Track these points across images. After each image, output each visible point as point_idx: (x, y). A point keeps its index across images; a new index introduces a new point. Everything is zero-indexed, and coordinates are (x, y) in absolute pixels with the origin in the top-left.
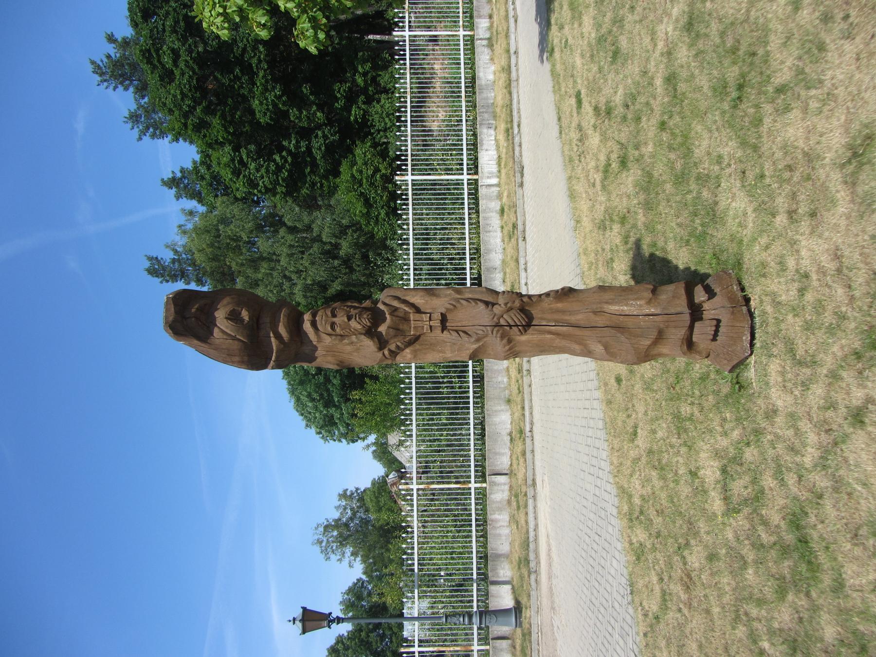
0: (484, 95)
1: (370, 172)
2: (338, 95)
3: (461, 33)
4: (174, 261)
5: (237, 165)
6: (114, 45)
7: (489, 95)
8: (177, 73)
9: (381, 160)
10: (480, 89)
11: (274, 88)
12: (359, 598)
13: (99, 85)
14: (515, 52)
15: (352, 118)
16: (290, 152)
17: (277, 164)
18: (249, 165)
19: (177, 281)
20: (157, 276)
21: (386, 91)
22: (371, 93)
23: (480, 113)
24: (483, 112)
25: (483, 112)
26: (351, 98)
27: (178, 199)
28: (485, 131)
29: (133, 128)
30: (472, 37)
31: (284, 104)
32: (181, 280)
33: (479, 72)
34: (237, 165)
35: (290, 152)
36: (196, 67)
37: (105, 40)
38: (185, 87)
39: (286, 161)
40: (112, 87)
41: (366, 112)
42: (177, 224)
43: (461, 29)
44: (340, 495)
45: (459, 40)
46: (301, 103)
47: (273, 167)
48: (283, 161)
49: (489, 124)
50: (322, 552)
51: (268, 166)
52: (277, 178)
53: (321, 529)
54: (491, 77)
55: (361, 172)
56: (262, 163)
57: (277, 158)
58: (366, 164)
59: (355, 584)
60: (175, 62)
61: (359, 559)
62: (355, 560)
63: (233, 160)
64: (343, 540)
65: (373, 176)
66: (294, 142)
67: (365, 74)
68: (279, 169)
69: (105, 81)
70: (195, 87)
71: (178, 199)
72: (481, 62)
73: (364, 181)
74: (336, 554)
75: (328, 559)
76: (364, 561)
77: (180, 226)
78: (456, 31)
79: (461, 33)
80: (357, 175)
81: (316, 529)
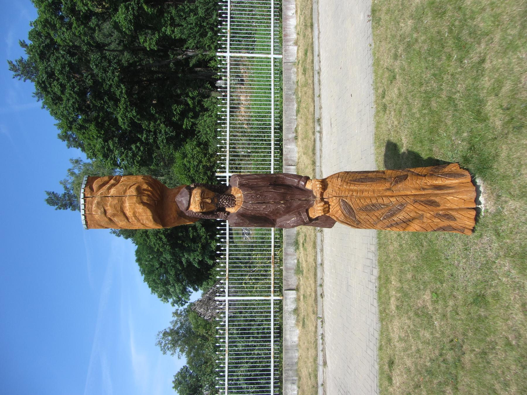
0: (290, 355)
1: (196, 163)
2: (175, 113)
3: (272, 298)
4: (65, 195)
5: (106, 151)
6: (25, 49)
7: (294, 355)
8: (65, 99)
9: (203, 156)
10: (286, 350)
11: (132, 110)
12: (184, 377)
13: (14, 78)
14: (322, 385)
15: (184, 127)
16: (142, 143)
17: (133, 152)
18: (114, 152)
19: (67, 209)
20: (53, 205)
21: (207, 110)
22: (197, 110)
23: (286, 370)
24: (288, 370)
25: (288, 370)
26: (183, 115)
27: (69, 147)
28: (289, 386)
29: (38, 101)
30: (281, 301)
31: (138, 119)
32: (69, 207)
33: (286, 335)
34: (106, 151)
35: (142, 143)
36: (77, 98)
37: (19, 45)
38: (70, 109)
39: (139, 150)
40: (23, 79)
41: (194, 124)
42: (68, 169)
43: (272, 294)
44: (173, 313)
45: (270, 304)
46: (151, 118)
47: (130, 154)
48: (137, 150)
49: (293, 380)
50: (161, 350)
51: (127, 153)
52: (133, 161)
53: (161, 335)
54: (296, 339)
55: (189, 162)
56: (123, 151)
57: (133, 147)
58: (193, 157)
59: (182, 369)
60: (63, 92)
61: (184, 354)
62: (182, 354)
63: (103, 147)
64: (174, 343)
65: (197, 166)
66: (145, 136)
67: (193, 98)
68: (134, 155)
69: (18, 75)
70: (77, 109)
71: (69, 147)
72: (288, 326)
73: (192, 169)
74: (170, 351)
75: (165, 353)
76: (188, 354)
77: (69, 170)
78: (267, 296)
79: (272, 298)
80: (188, 165)
81: (158, 335)
